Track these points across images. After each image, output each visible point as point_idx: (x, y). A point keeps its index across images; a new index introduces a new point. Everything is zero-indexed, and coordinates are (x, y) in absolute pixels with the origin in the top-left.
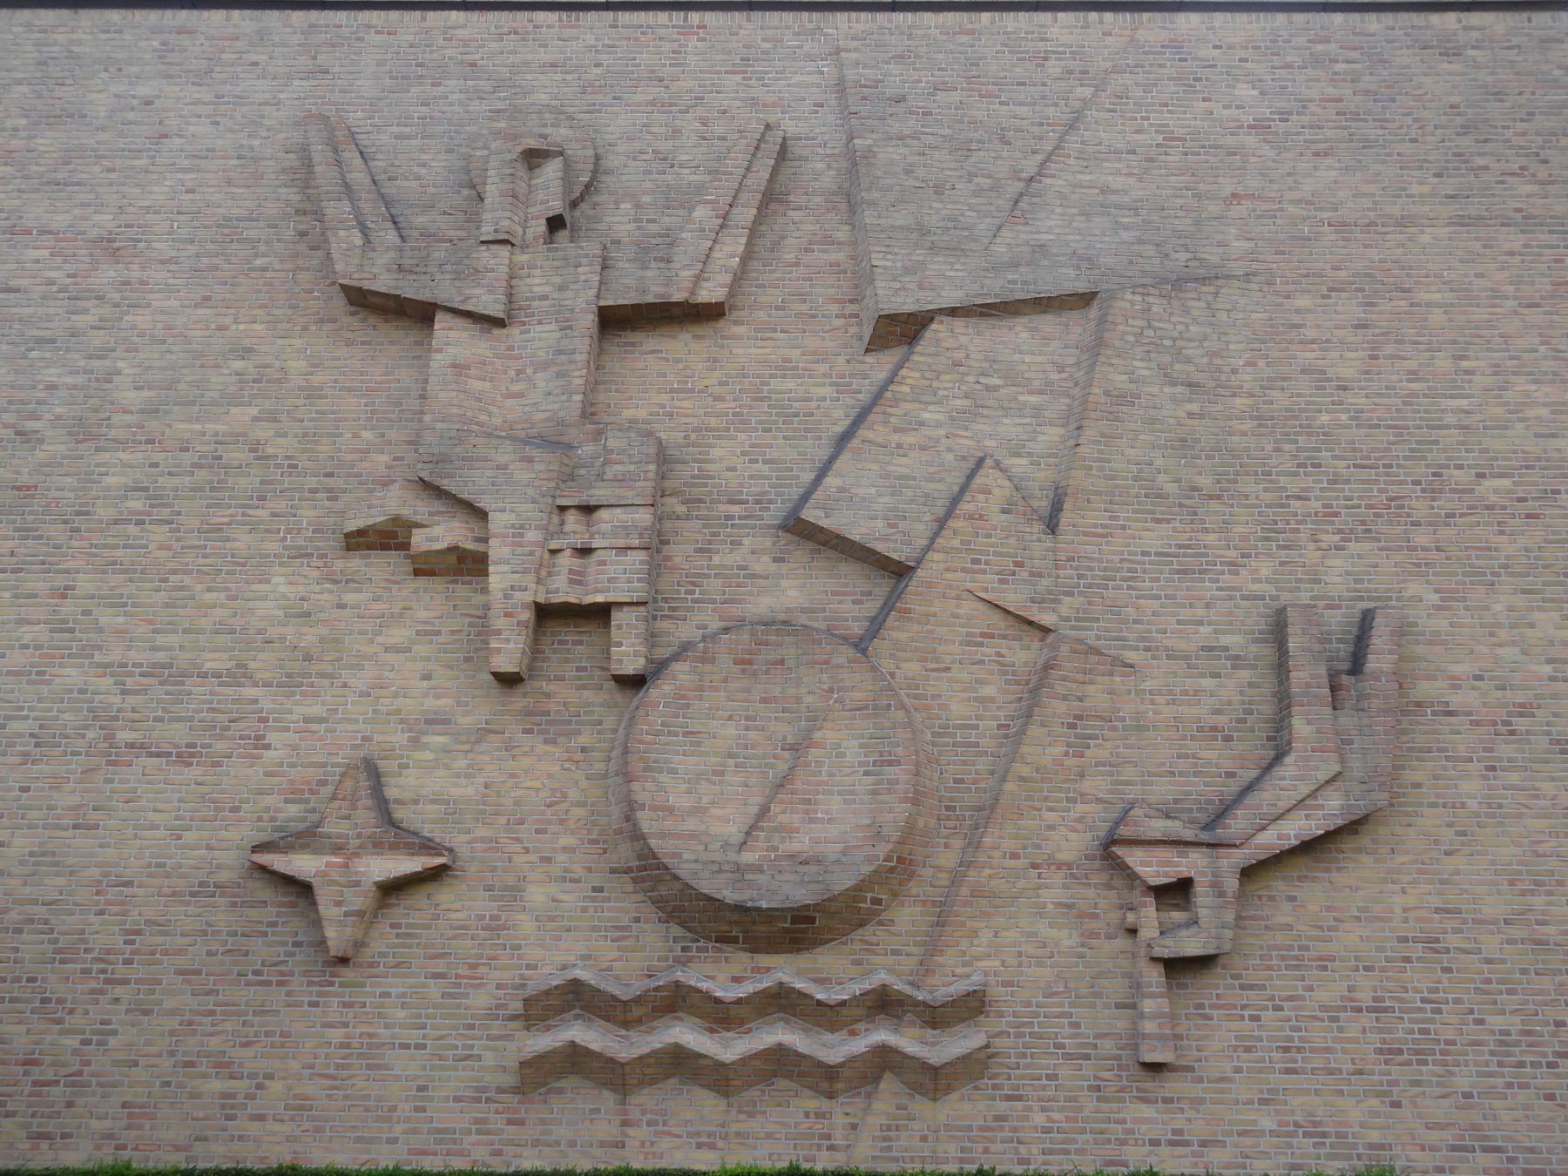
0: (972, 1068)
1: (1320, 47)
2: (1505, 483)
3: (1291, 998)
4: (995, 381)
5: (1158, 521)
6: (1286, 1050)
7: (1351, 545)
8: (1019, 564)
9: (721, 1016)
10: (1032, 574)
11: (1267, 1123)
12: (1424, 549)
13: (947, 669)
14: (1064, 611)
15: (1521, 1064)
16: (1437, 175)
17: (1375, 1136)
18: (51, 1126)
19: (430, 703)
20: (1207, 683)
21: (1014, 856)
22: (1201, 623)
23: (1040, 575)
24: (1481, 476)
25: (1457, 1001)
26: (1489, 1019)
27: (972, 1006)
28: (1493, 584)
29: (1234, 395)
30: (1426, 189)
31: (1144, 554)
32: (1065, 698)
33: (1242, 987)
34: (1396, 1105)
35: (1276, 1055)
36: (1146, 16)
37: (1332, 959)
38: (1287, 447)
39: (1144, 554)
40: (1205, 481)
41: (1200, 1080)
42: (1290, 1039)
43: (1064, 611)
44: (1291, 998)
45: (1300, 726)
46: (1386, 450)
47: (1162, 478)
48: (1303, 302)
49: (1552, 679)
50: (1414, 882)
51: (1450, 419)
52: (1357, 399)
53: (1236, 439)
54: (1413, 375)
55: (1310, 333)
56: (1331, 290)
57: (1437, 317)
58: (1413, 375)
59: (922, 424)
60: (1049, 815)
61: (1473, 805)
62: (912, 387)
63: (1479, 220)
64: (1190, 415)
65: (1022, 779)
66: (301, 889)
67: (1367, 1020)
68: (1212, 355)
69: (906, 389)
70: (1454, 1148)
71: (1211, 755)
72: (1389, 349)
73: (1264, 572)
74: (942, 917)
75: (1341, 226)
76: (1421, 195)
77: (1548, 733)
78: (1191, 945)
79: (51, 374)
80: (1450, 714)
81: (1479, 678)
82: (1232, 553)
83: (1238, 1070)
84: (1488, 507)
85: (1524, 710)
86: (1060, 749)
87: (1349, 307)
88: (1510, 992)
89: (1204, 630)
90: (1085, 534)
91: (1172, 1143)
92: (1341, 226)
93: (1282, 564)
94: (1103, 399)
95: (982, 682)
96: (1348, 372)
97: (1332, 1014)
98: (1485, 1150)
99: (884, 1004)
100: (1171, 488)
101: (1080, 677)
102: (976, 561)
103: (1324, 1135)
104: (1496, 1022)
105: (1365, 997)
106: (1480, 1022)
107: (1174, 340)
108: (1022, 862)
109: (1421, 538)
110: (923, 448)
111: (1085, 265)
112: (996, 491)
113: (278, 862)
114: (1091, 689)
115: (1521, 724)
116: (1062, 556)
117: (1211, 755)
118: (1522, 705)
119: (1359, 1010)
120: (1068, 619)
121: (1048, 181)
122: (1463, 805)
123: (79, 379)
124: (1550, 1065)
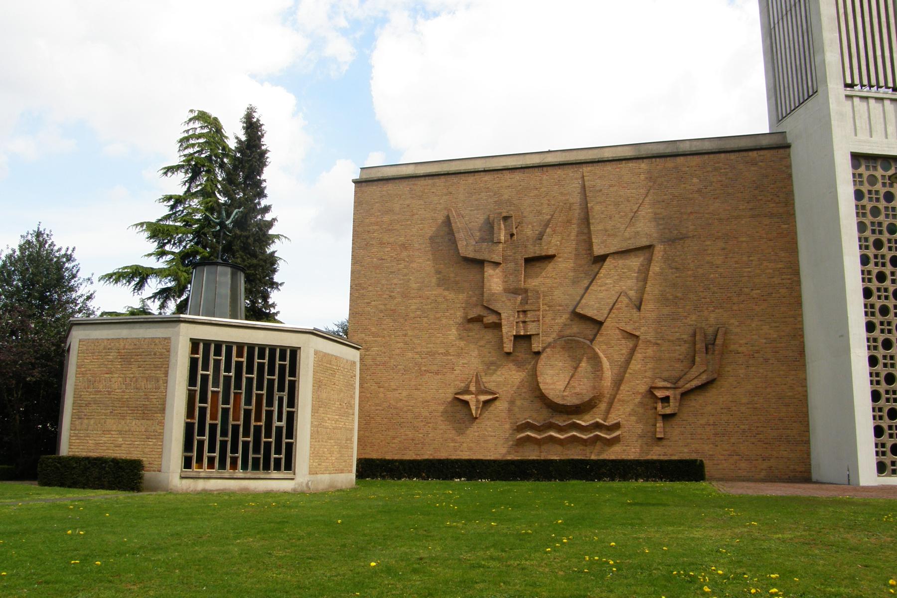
0: (617, 440)
1: (717, 165)
2: (759, 291)
4: (625, 270)
6: (692, 434)
9: (560, 429)
10: (634, 322)
13: (613, 347)
14: (642, 331)
15: (747, 436)
16: (748, 203)
17: (711, 453)
19: (491, 359)
20: (678, 348)
21: (628, 391)
24: (752, 290)
25: (734, 422)
27: (617, 426)
30: (744, 207)
32: (641, 353)
34: (717, 446)
40: (679, 295)
41: (670, 441)
43: (642, 331)
45: (697, 359)
47: (668, 295)
48: (708, 243)
49: (766, 343)
51: (745, 274)
54: (736, 262)
55: (709, 252)
57: (744, 245)
58: (736, 262)
60: (637, 381)
63: (759, 215)
64: (676, 277)
66: (466, 403)
67: (712, 427)
68: (682, 260)
69: (602, 275)
70: (729, 455)
72: (731, 255)
74: (611, 404)
75: (720, 220)
76: (743, 209)
78: (668, 411)
79: (395, 281)
82: (686, 314)
83: (680, 439)
84: (754, 298)
85: (758, 352)
87: (721, 244)
91: (664, 455)
92: (720, 220)
94: (653, 275)
96: (719, 262)
97: (703, 426)
99: (597, 426)
100: (671, 297)
102: (619, 320)
104: (742, 427)
105: (711, 422)
106: (739, 427)
107: (672, 256)
108: (631, 393)
109: (735, 308)
110: (607, 290)
111: (649, 237)
113: (461, 397)
114: (648, 350)
115: (756, 355)
119: (709, 425)
123: (402, 282)
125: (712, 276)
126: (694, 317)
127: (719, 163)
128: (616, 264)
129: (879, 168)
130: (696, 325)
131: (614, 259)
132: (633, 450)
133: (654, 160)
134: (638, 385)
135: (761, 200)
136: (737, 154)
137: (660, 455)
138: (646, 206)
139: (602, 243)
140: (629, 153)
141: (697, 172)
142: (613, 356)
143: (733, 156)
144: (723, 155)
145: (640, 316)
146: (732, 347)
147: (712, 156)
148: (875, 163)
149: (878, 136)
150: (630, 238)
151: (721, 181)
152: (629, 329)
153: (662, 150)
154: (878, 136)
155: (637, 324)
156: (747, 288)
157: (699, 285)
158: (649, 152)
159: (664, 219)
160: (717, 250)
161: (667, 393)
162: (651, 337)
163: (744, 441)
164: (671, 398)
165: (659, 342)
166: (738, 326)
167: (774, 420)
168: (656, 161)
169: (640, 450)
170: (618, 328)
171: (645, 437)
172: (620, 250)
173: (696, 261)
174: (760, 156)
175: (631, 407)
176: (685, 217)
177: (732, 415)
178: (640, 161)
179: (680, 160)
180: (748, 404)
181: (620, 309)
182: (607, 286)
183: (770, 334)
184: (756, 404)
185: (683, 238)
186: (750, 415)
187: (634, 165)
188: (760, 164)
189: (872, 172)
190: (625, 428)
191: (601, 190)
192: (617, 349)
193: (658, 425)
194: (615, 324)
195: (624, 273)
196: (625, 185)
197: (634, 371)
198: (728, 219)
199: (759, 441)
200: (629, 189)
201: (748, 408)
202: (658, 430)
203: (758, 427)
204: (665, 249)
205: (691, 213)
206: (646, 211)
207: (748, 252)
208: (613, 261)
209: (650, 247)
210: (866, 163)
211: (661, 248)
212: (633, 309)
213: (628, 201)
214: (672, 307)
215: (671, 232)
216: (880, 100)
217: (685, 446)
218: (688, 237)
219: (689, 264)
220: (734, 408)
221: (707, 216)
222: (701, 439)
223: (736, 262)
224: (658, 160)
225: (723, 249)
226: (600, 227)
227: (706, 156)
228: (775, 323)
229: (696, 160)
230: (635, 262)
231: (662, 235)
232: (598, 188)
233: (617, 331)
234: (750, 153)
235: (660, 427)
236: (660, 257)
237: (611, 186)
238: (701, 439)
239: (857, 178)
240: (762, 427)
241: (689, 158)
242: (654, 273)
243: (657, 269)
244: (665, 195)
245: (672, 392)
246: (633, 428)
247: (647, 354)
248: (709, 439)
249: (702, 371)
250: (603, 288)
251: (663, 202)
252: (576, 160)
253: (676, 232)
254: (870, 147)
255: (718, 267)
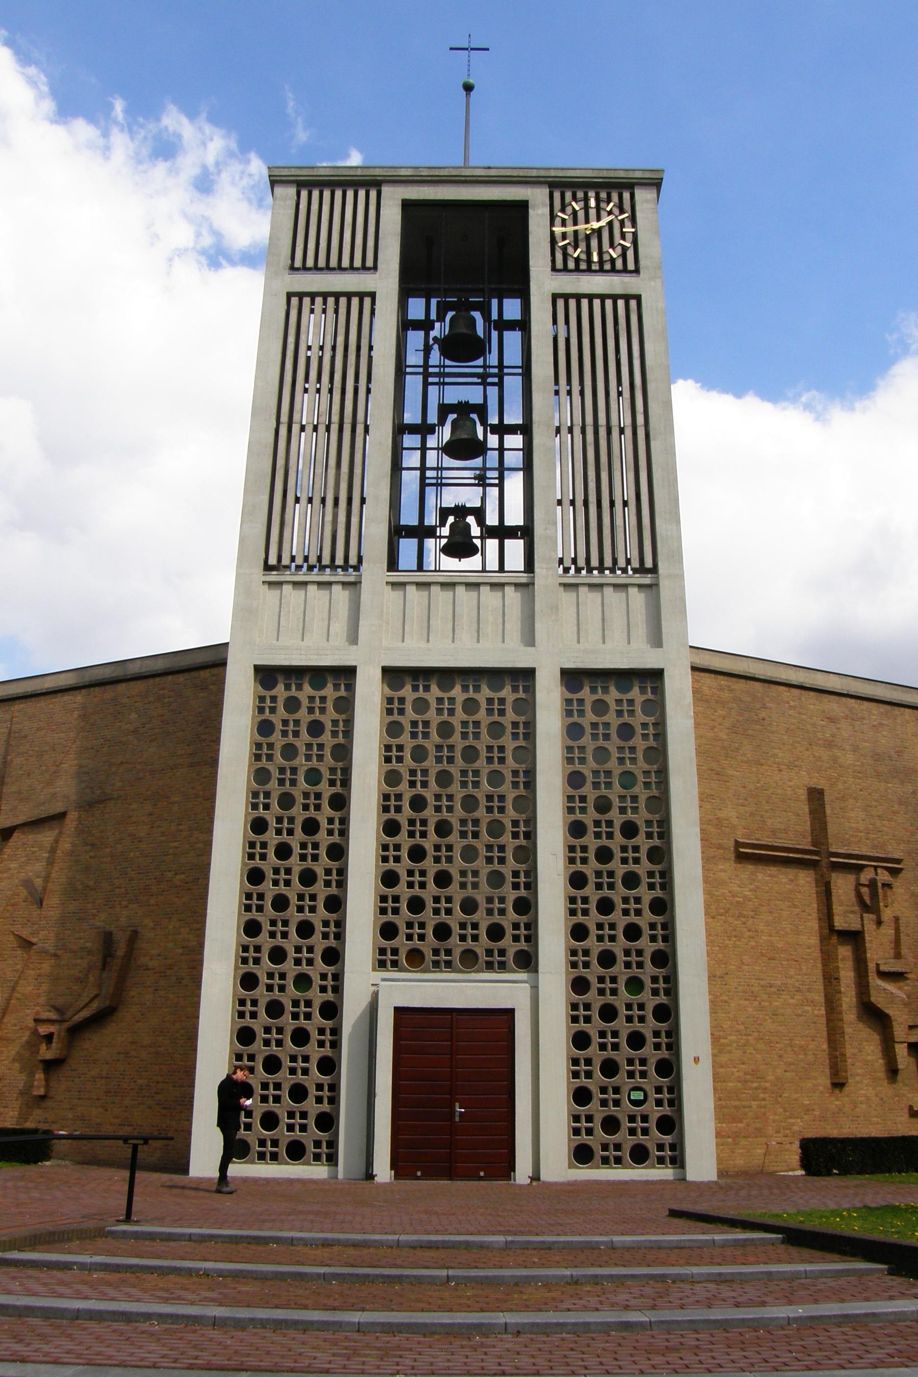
1: (161, 692)
2: (183, 876)
3: (83, 1074)
4: (36, 849)
5: (74, 900)
6: (79, 1091)
7: (130, 905)
8: (28, 921)
10: (32, 924)
11: (70, 1116)
12: (153, 905)
13: (6, 960)
14: (40, 936)
15: (144, 1097)
16: (188, 745)
17: (98, 1120)
18: (811, 1354)
20: (79, 961)
21: (15, 1025)
22: (81, 939)
23: (35, 924)
24: (176, 874)
25: (130, 1075)
26: (138, 1081)
28: (170, 918)
29: (106, 847)
30: (183, 752)
31: (69, 913)
32: (33, 969)
33: (72, 1070)
34: (106, 1110)
35: (76, 1093)
36: (108, 686)
37: (97, 1060)
38: (118, 867)
39: (69, 913)
40: (91, 883)
41: (54, 1101)
42: (81, 1088)
43: (40, 936)
44: (83, 1074)
46: (149, 866)
47: (78, 883)
49: (182, 954)
50: (125, 1033)
52: (143, 846)
53: (103, 865)
54: (163, 834)
55: (134, 819)
56: (145, 800)
58: (163, 834)
59: (10, 869)
60: (27, 1011)
61: (148, 1003)
62: (9, 855)
64: (91, 857)
65: (18, 999)
67: (103, 1081)
68: (102, 832)
69: (6, 856)
70: (120, 1125)
71: (75, 988)
72: (157, 823)
73: (103, 918)
76: (181, 755)
77: (176, 976)
80: (148, 969)
81: (159, 955)
82: (94, 911)
83: (65, 1098)
84: (176, 887)
85: (170, 967)
86: (32, 988)
88: (146, 1071)
89: (82, 941)
90: (52, 907)
91: (44, 1122)
93: (109, 914)
94: (61, 855)
95: (16, 964)
96: (142, 834)
98: (128, 1125)
100: (80, 887)
101: (39, 961)
102: (14, 921)
103: (85, 1120)
104: (140, 1081)
105: (104, 1073)
106: (135, 1082)
107: (88, 827)
108: (18, 1027)
109: (152, 902)
110: (9, 878)
111: (66, 800)
112: (22, 894)
114: (44, 965)
115: (169, 972)
116: (42, 916)
117: (75, 988)
118: (170, 965)
119: (102, 1078)
120: (40, 940)
121: (63, 765)
122: (145, 1004)
124: (152, 1097)
125: (132, 854)
126: (103, 916)
127: (163, 689)
128: (25, 840)
129: (612, 689)
130: (104, 928)
131: (24, 833)
132: (11, 1114)
133: (92, 689)
134: (27, 1015)
135: (205, 740)
136: (187, 675)
137: (40, 1122)
138: (71, 756)
139: (11, 810)
140: (70, 681)
141: (137, 704)
142: (5, 973)
143: (181, 678)
144: (170, 678)
145: (40, 915)
146: (143, 960)
147: (157, 680)
148: (301, 679)
149: (466, 637)
150: (44, 803)
151: (163, 716)
152: (25, 933)
153: (107, 674)
154: (466, 637)
155: (36, 926)
156: (169, 871)
157: (115, 869)
158: (93, 679)
159: (89, 773)
160: (143, 816)
161: (52, 1029)
162: (50, 946)
163: (139, 1104)
164: (55, 1037)
165: (59, 952)
166: (153, 929)
167: (179, 1072)
168: (94, 691)
169: (19, 1114)
170: (13, 932)
171: (26, 1093)
172: (30, 820)
173: (117, 833)
174: (213, 675)
175: (17, 1049)
176: (114, 769)
177: (129, 1064)
178: (77, 692)
179: (122, 687)
180: (150, 1046)
181: (16, 905)
182: (11, 872)
183: (188, 941)
184: (160, 1047)
185: (103, 800)
186: (151, 1064)
187: (70, 698)
188: (211, 687)
189: (471, 694)
190: (6, 1079)
191: (25, 737)
192: (11, 962)
193: (37, 1076)
194: (10, 926)
195: (33, 852)
196: (54, 727)
197: (23, 995)
198: (163, 770)
199: (157, 1104)
200: (58, 733)
201: (149, 1054)
202: (36, 1083)
203: (158, 1082)
204: (79, 817)
205: (122, 763)
206: (70, 764)
207: (178, 818)
208: (23, 836)
209: (62, 816)
210: (285, 679)
211: (74, 815)
212: (32, 905)
213: (54, 750)
214: (81, 901)
215: (93, 793)
216: (324, 585)
217: (71, 1109)
218: (112, 799)
219: (108, 838)
220: (133, 1053)
221: (139, 767)
222: (90, 1099)
223: (163, 833)
224: (97, 689)
225: (151, 815)
226: (14, 788)
227: (151, 681)
228: (197, 923)
229: (140, 686)
230: (46, 837)
231: (81, 797)
232: (23, 734)
233: (12, 938)
234: (202, 673)
235: (40, 1079)
236: (73, 829)
237: (39, 729)
238: (90, 1099)
239: (391, 706)
240: (163, 1082)
241: (132, 683)
242: (63, 852)
243: (68, 846)
244: (96, 739)
245: (58, 1027)
246: (15, 1080)
247: (42, 971)
248: (98, 1099)
249: (92, 995)
250: (5, 875)
251: (92, 749)
252: (8, 695)
253: (98, 792)
254: (287, 657)
255: (140, 842)
